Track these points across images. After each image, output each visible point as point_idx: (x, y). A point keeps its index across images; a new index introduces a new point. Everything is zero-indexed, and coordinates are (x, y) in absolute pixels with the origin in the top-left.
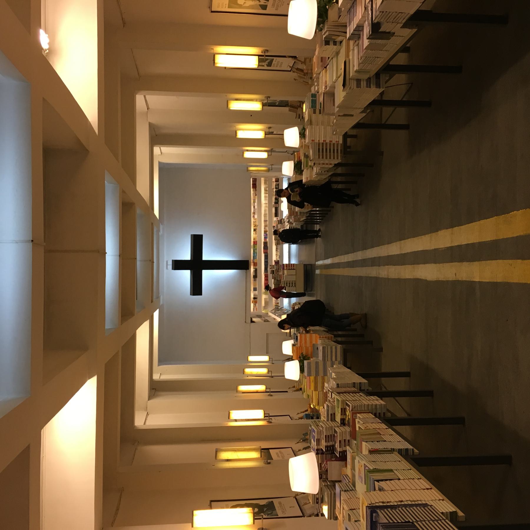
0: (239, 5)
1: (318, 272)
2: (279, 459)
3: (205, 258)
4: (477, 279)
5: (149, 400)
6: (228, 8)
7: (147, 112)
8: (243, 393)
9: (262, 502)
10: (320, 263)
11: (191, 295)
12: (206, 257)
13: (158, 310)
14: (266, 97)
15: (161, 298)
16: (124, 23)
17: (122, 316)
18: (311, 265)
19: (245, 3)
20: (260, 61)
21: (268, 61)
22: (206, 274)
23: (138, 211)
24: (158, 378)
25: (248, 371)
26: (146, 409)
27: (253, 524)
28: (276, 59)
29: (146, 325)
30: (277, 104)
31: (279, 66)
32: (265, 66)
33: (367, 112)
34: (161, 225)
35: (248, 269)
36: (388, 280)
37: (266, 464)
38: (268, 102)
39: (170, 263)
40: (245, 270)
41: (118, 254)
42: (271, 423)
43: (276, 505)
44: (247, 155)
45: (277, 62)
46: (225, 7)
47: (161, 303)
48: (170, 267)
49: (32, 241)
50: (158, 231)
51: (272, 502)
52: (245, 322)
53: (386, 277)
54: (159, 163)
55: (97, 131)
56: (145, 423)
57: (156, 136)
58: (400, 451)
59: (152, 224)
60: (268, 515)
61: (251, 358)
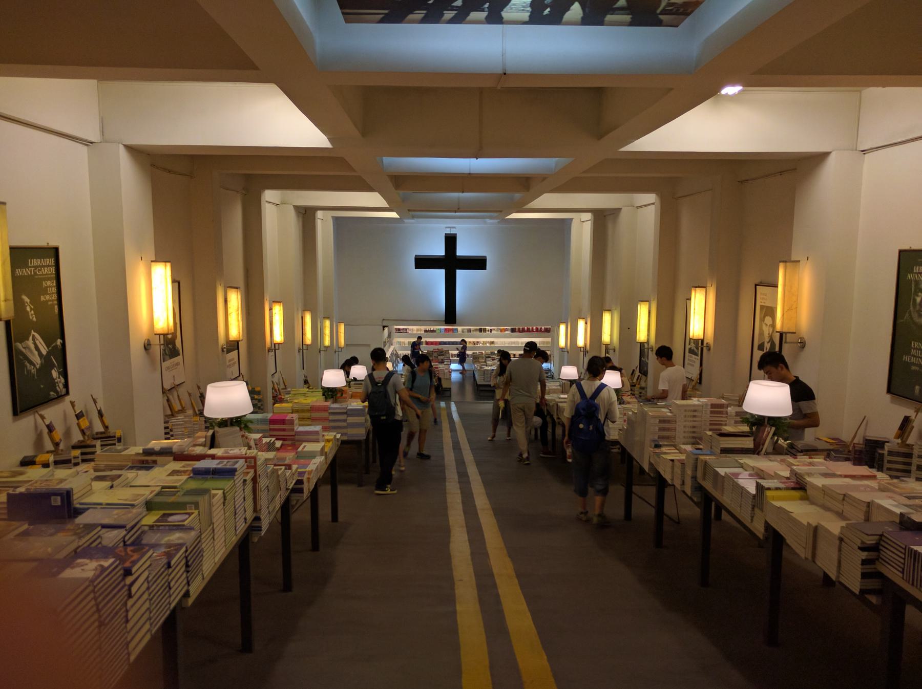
0: (764, 317)
1: (443, 404)
2: (227, 361)
3: (459, 272)
4: (458, 608)
5: (294, 206)
6: (761, 306)
7: (634, 206)
8: (302, 317)
9: (178, 342)
10: (453, 407)
11: (416, 256)
12: (461, 274)
13: (398, 217)
14: (652, 347)
15: (413, 221)
16: (742, 182)
17: (395, 176)
18: (450, 396)
19: (767, 325)
20: (696, 341)
21: (695, 350)
22: (441, 273)
23: (518, 196)
24: (318, 217)
25: (327, 323)
26: (283, 203)
27: (156, 333)
28: (698, 359)
29: (383, 203)
30: (642, 359)
31: (689, 362)
32: (690, 346)
33: (650, 474)
34: (498, 220)
35: (446, 323)
36: (444, 493)
37: (222, 346)
38: (645, 350)
39: (453, 232)
40: (444, 320)
41: (472, 172)
42: (269, 351)
43: (178, 359)
44: (581, 324)
45: (694, 360)
46: (761, 302)
47: (406, 221)
48: (448, 231)
49: (505, 74)
50: (491, 218)
51: (179, 355)
52: (384, 320)
53: (447, 491)
54: (571, 219)
55: (623, 149)
56: (267, 202)
57: (605, 216)
58: (257, 519)
59: (501, 211)
60: (164, 350)
61: (342, 328)
